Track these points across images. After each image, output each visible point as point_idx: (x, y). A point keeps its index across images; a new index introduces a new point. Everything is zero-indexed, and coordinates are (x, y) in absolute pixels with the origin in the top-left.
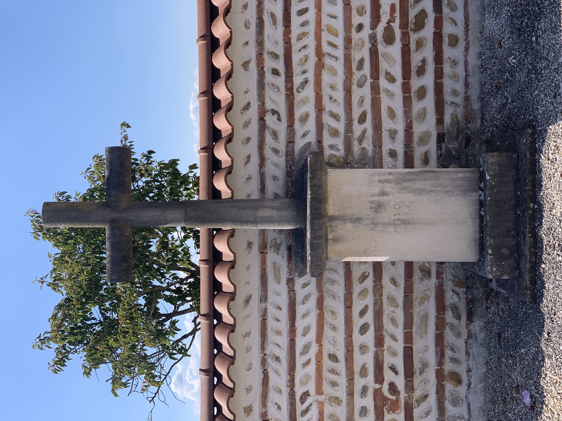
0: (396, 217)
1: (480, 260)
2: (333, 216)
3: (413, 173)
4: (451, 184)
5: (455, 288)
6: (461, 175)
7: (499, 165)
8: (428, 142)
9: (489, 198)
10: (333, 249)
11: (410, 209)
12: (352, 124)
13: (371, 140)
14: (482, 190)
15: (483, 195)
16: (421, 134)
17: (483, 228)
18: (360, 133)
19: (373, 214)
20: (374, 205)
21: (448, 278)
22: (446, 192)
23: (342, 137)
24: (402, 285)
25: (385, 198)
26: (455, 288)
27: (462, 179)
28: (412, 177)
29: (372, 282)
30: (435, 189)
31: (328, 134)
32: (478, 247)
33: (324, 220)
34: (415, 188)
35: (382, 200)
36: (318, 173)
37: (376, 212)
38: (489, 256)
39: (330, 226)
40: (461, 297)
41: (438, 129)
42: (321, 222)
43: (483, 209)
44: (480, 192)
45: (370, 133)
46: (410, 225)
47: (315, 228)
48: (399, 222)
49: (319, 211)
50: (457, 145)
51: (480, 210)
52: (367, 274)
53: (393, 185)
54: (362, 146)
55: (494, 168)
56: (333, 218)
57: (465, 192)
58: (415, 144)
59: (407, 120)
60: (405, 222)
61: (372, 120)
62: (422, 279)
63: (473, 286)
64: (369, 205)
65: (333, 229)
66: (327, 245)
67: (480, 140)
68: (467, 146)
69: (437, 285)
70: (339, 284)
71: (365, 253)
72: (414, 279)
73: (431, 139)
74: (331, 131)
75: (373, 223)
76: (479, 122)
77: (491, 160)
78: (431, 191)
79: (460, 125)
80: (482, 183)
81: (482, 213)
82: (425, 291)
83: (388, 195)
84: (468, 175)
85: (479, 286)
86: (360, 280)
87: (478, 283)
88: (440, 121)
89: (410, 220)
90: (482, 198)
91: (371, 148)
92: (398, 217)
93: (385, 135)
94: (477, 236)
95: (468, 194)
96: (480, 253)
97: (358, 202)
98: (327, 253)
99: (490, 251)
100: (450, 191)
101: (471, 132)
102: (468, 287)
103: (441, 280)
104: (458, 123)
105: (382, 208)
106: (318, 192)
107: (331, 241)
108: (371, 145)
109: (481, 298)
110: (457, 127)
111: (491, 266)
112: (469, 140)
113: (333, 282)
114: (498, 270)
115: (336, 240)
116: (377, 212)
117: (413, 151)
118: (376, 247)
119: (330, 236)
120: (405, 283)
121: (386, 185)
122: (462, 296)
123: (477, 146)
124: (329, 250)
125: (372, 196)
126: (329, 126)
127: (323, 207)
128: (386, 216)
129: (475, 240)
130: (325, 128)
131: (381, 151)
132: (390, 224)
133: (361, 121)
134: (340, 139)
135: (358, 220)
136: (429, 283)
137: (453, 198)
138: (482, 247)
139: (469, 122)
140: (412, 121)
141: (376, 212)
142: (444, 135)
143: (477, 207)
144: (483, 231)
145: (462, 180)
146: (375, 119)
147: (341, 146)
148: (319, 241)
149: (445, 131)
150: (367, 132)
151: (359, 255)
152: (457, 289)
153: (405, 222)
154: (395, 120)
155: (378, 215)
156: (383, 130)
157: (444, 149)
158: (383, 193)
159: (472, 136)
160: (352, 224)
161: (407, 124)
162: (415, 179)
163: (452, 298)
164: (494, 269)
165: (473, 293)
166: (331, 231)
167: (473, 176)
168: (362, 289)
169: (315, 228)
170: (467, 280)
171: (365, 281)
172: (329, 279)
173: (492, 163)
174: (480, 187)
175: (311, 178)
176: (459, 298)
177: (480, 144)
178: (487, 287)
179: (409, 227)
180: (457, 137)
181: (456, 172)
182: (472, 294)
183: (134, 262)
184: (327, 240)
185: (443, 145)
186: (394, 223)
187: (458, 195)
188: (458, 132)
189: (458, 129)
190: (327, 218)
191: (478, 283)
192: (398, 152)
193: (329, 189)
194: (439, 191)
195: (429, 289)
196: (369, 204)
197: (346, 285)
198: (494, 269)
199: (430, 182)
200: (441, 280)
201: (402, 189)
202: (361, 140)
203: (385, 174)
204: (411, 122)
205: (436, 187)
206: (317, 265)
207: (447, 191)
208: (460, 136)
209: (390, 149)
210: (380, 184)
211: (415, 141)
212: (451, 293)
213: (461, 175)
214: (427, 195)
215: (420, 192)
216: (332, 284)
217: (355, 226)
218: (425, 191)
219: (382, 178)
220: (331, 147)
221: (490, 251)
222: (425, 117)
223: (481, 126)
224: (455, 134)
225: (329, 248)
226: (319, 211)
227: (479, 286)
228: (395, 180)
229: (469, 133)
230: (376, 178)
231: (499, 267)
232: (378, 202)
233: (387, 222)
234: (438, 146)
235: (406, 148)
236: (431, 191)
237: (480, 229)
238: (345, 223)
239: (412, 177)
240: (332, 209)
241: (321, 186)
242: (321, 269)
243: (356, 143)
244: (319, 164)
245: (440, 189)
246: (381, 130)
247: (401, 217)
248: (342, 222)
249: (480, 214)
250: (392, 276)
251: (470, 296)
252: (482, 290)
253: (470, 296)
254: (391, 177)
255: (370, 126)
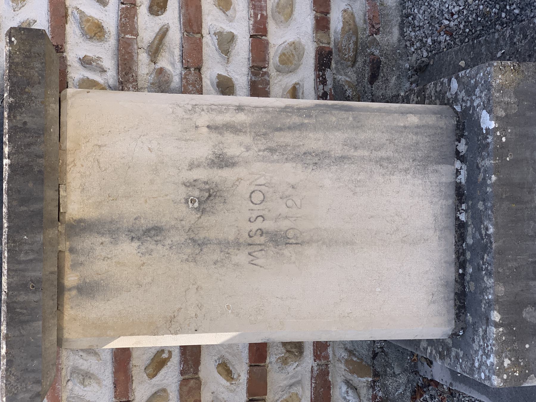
0: (255, 227)
1: (454, 335)
2: (80, 221)
3: (299, 109)
4: (391, 141)
5: (349, 376)
6: (413, 120)
7: (517, 93)
8: (297, 67)
9: (494, 178)
10: (78, 318)
11: (290, 203)
12: (135, 14)
13: (177, 52)
14: (462, 158)
15: (464, 173)
16: (285, 48)
17: (464, 253)
18: (153, 35)
19: (194, 217)
20: (197, 193)
21: (338, 355)
22: (379, 161)
23: (112, 41)
24: (244, 377)
25: (227, 173)
26: (349, 376)
27: (418, 129)
28: (296, 119)
29: (177, 373)
30: (352, 152)
31: (78, 32)
32: (452, 302)
33: (51, 233)
34: (303, 150)
35: (217, 179)
36: (34, 91)
37: (201, 211)
38: (494, 330)
39: (72, 250)
40: (362, 395)
41: (318, 41)
42: (40, 238)
43: (464, 206)
44: (458, 164)
45: (175, 36)
46: (291, 248)
47: (22, 257)
48: (262, 239)
49: (35, 207)
50: (354, 77)
51: (457, 209)
52: (165, 356)
53: (247, 139)
54: (159, 65)
55: (506, 99)
56: (80, 227)
57: (424, 163)
58: (271, 69)
59: (256, 15)
60: (279, 240)
61: (180, 8)
62: (284, 361)
63: (385, 371)
64: (182, 192)
65: (82, 259)
66: (59, 307)
67: (398, 69)
68: (373, 78)
69: (315, 373)
70: (99, 383)
71: (171, 325)
72: (268, 361)
73: (304, 60)
74: (86, 26)
75: (194, 241)
76: (396, 31)
77: (498, 80)
78: (343, 158)
79: (360, 36)
80: (463, 141)
81: (463, 217)
82: (291, 386)
83: (233, 165)
84: (431, 120)
85: (397, 371)
86: (150, 371)
87: (395, 365)
88: (322, 24)
89: (290, 234)
90: (463, 178)
91: (178, 72)
92: (259, 224)
93: (209, 45)
94: (451, 274)
95: (431, 168)
96: (458, 316)
97: (152, 182)
98: (60, 329)
99: (496, 316)
100: (388, 159)
101: (381, 51)
102: (376, 374)
103: (323, 362)
104: (356, 32)
105: (217, 200)
106: (35, 149)
107: (74, 292)
108: (179, 65)
109: (402, 395)
110: (354, 39)
111: (499, 355)
112: (379, 67)
113: (86, 377)
114: (515, 364)
115: (87, 290)
116: (203, 211)
117: (268, 83)
118: (200, 307)
119: (71, 279)
120: (250, 373)
121: (229, 137)
122: (364, 392)
123: (393, 80)
124: (66, 318)
125: (192, 166)
126: (81, 13)
127: (50, 194)
128: (227, 222)
129: (447, 285)
130: (70, 19)
131: (201, 79)
132: (238, 244)
133: (155, 8)
134: (106, 45)
135: (149, 233)
136: (299, 368)
137: (396, 178)
138: (464, 300)
139: (378, 29)
140: (266, 17)
141: (201, 211)
142: (330, 53)
143: (450, 202)
144: (465, 261)
145: (417, 134)
146: (187, 5)
147: (109, 62)
148: (33, 298)
149: (332, 46)
150: (170, 34)
151: (155, 332)
152: (357, 380)
153: (279, 240)
154: (229, 13)
155: (207, 220)
156: (205, 31)
157: (329, 82)
158: (221, 161)
159: (383, 59)
160: (136, 244)
161: (255, 22)
162: (302, 125)
163: (345, 398)
164: (507, 362)
165: (385, 385)
166: (75, 266)
167: (442, 123)
168: (154, 390)
169: (22, 257)
170: (374, 358)
171: (163, 372)
172: (75, 371)
173: (501, 88)
174: (457, 152)
175: (11, 107)
176: (359, 397)
177: (398, 77)
178: (416, 373)
179: (287, 251)
180: (355, 62)
181: (404, 113)
182: (384, 386)
183: (477, 154)
184: (61, 289)
185: (328, 74)
186: (250, 241)
187: (406, 171)
188: (356, 50)
189: (356, 43)
190: (61, 228)
191: (395, 365)
192: (236, 82)
193: (69, 145)
194: (363, 158)
195: (299, 382)
196: (183, 190)
197: (116, 385)
198: (507, 362)
199: (339, 136)
200: (323, 362)
201: (272, 150)
202: (155, 50)
203: (227, 110)
204: (264, 18)
205: (356, 148)
206: (26, 370)
207: (382, 159)
208: (359, 59)
209: (219, 76)
210: (215, 136)
211: (271, 62)
212: (344, 388)
213: (413, 120)
214: (334, 168)
215: (318, 159)
216: (83, 383)
217: (143, 249)
218: (329, 157)
219: (220, 119)
220: (86, 62)
221: (496, 316)
222: (292, 11)
223: (399, 41)
224: (352, 54)
225: (70, 312)
226: (35, 207)
227: (397, 371)
228: (253, 125)
229: (377, 53)
230: (203, 120)
231: (518, 355)
232: (206, 183)
233: (231, 238)
234: (318, 76)
235: (254, 74)
236: (343, 158)
237: (458, 258)
238: (115, 242)
239: (296, 119)
240: (76, 204)
241: (41, 132)
242: (38, 382)
243: (143, 58)
244: (38, 65)
245: (366, 153)
246: (200, 32)
247: (269, 225)
248: (106, 239)
249: (457, 219)
250: (222, 357)
251: (380, 394)
252: (403, 379)
253: (380, 394)
254: (241, 117)
255: (177, 21)
